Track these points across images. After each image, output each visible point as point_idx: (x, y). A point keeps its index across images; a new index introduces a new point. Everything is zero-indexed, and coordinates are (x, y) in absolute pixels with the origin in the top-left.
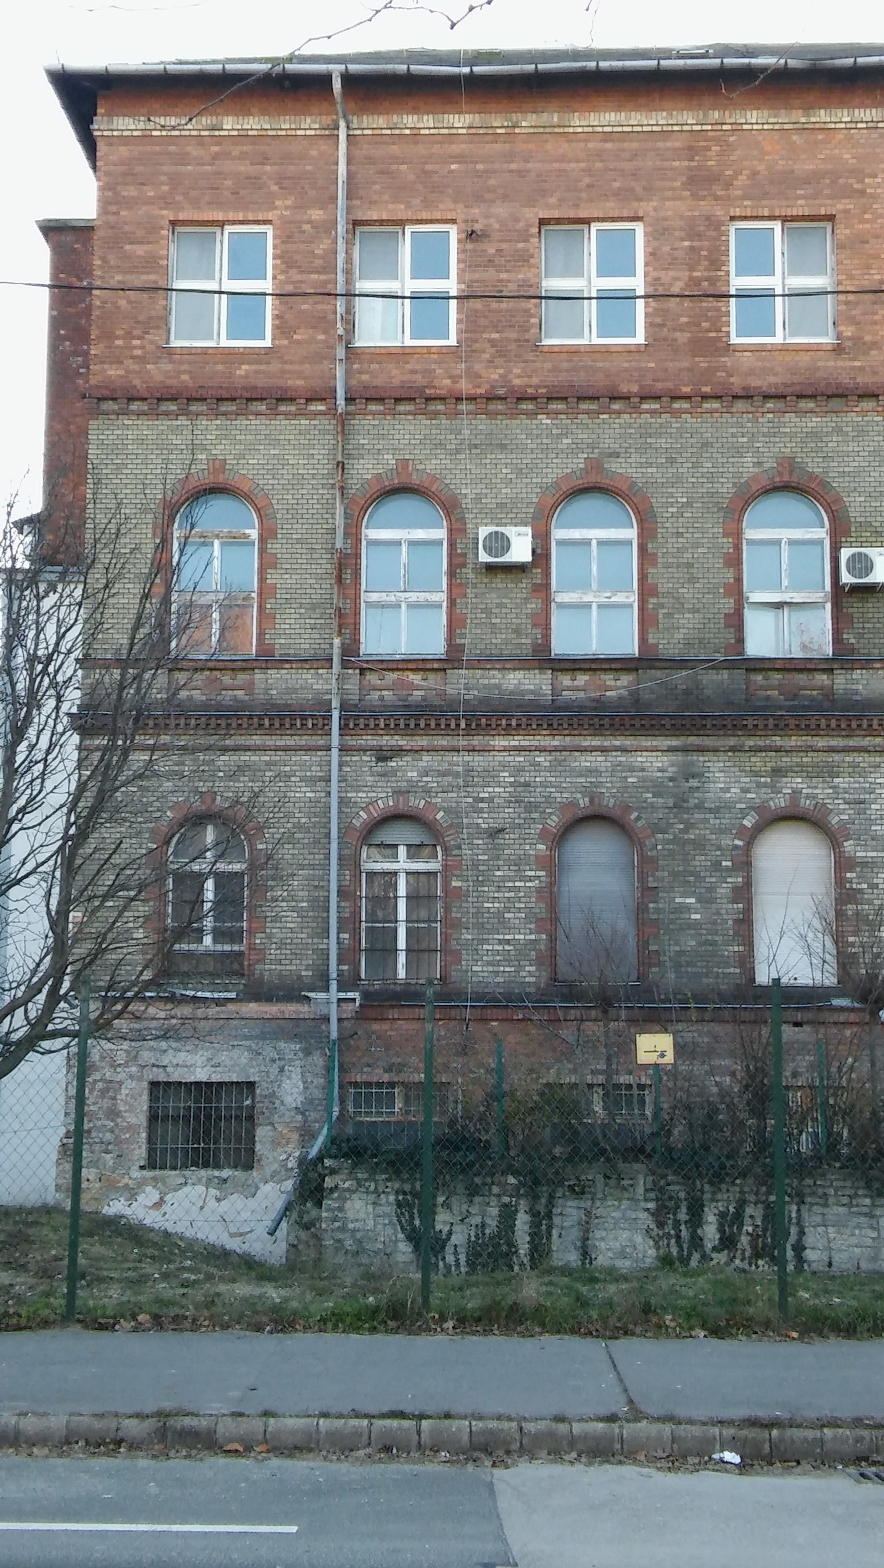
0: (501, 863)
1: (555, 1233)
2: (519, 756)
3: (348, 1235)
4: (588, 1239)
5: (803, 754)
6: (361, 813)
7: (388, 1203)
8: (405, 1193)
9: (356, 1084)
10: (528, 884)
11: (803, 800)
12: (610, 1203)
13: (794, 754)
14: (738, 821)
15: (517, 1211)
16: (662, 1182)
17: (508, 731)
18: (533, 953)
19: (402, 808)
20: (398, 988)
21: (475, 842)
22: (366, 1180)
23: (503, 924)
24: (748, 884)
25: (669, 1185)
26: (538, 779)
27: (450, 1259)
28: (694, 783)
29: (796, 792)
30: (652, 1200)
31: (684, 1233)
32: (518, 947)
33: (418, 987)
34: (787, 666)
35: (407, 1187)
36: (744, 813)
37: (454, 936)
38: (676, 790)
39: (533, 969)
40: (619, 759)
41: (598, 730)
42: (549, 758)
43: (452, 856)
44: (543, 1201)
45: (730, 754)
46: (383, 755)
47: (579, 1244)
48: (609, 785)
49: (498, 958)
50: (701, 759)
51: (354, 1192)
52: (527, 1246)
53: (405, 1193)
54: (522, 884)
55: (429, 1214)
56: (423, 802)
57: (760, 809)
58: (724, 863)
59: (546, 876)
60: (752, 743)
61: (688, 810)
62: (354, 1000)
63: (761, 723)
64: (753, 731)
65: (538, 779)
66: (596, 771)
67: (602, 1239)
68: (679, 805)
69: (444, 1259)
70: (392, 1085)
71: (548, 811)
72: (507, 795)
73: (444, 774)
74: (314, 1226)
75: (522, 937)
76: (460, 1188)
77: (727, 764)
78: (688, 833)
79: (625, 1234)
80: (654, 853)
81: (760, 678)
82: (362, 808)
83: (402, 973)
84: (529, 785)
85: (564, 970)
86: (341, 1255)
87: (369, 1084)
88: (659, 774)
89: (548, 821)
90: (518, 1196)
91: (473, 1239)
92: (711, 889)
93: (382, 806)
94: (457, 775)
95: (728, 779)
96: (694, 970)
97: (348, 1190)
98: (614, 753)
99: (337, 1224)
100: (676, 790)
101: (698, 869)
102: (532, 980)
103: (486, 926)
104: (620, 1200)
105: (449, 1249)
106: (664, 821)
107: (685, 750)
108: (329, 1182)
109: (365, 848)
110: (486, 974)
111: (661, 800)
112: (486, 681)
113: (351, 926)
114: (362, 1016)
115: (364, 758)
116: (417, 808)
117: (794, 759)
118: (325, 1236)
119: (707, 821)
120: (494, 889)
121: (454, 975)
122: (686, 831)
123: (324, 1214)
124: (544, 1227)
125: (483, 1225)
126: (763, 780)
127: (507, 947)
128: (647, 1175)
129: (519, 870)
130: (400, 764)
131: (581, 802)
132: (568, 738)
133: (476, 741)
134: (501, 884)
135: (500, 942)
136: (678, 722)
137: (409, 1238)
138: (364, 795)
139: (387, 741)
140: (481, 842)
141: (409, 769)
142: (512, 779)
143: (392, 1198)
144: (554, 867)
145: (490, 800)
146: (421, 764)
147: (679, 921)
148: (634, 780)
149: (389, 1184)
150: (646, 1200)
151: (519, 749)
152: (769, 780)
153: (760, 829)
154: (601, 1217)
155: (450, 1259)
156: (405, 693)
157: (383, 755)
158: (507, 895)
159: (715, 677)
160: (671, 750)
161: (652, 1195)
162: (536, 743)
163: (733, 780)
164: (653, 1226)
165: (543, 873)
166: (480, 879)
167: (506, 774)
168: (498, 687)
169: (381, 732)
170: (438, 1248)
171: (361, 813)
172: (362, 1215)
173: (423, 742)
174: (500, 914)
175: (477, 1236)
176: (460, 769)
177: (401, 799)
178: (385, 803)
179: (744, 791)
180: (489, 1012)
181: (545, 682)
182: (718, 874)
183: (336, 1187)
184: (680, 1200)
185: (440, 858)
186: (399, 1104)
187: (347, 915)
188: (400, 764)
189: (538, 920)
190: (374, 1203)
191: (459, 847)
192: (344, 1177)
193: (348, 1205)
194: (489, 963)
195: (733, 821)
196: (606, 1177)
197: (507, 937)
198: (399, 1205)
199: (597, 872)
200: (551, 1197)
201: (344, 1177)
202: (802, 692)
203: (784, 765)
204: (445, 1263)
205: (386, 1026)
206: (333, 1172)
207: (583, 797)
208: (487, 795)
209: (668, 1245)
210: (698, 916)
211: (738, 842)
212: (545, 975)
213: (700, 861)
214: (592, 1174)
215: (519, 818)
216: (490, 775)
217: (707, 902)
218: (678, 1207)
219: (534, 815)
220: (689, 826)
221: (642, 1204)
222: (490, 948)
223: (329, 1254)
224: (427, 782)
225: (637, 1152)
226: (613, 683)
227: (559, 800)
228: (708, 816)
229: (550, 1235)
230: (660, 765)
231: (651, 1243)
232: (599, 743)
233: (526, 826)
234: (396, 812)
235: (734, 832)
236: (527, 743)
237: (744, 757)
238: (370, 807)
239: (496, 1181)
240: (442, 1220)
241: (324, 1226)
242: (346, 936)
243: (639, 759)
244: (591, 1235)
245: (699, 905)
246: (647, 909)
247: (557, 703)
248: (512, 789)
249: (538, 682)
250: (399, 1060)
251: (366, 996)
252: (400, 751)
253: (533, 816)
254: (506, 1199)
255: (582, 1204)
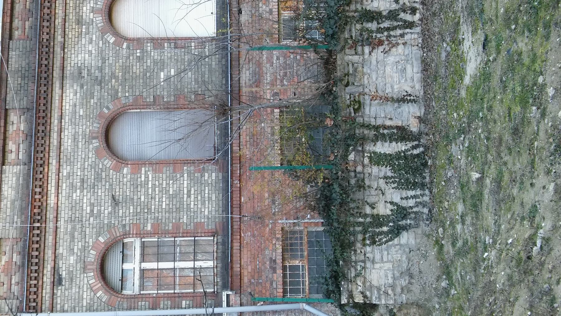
0: (135, 197)
1: (388, 123)
2: (62, 186)
3: (397, 282)
4: (392, 98)
5: (68, 5)
6: (98, 295)
7: (373, 251)
8: (364, 239)
9: (285, 292)
10: (150, 179)
11: (98, 6)
12: (366, 82)
13: (67, 11)
14: (111, 46)
15: (375, 153)
16: (350, 42)
17: (44, 193)
18: (196, 175)
19: (96, 266)
20: (219, 265)
21: (120, 215)
22: (356, 270)
23: (177, 195)
24: (153, 40)
25: (351, 37)
26: (79, 174)
27: (411, 203)
28: (85, 73)
29: (93, 10)
30: (363, 50)
31: (386, 24)
32: (192, 184)
33: (219, 251)
34: (9, 14)
35: (360, 237)
36: (106, 42)
37: (185, 227)
38: (89, 84)
39: (206, 175)
40: (67, 121)
41: (47, 134)
42: (65, 167)
43: (130, 231)
44: (366, 132)
45: (66, 50)
46: (57, 281)
47: (396, 105)
48: (84, 127)
49: (199, 198)
50: (69, 69)
51: (365, 278)
52: (399, 143)
53: (364, 239)
54: (150, 183)
55: (378, 220)
56: (92, 252)
57: (103, 33)
58: (138, 55)
59: (145, 167)
60: (59, 37)
61: (103, 77)
62: (228, 296)
63: (46, 30)
64: (52, 37)
65: (79, 174)
66: (74, 135)
67: (392, 87)
68: (100, 82)
69: (411, 208)
70: (284, 268)
71: (101, 167)
72: (89, 194)
73: (73, 237)
74: (392, 309)
75: (185, 182)
76: (359, 195)
77: (73, 52)
78: (118, 76)
79: (388, 69)
80: (131, 98)
81: (16, 33)
82: (95, 294)
83: (210, 264)
84: (83, 179)
85: (209, 153)
86: (413, 288)
87: (284, 283)
88: (78, 95)
89: (108, 166)
90: (363, 151)
91: (396, 185)
92: (155, 62)
93: (94, 281)
94: (74, 228)
95: (83, 51)
96: (207, 73)
97: (364, 283)
98: (63, 124)
99: (390, 292)
100: (89, 84)
101: (142, 70)
102: (214, 174)
103: (178, 206)
104: (364, 74)
105: (404, 203)
106: (110, 92)
107: (63, 78)
108: (359, 299)
109: (124, 292)
110: (210, 206)
111: (96, 94)
112: (8, 210)
113: (177, 299)
114: (239, 290)
115: (59, 294)
116: (95, 255)
117: (71, 11)
118: (399, 301)
119: (110, 65)
120: (153, 202)
121: (212, 227)
122: (116, 78)
123: (383, 302)
124: (386, 132)
125: (385, 178)
126: (84, 30)
127: (192, 192)
128: (345, 53)
129: (141, 185)
130: (64, 269)
131: (95, 145)
132: (51, 154)
133: (51, 215)
134: (150, 197)
135: (189, 196)
136: (43, 81)
137: (398, 234)
138: (85, 293)
139: (47, 279)
140: (121, 211)
141: (68, 262)
142: (78, 191)
143: (368, 249)
144: (139, 163)
145: (92, 205)
146: (65, 254)
147: (176, 83)
148: (81, 110)
149: (359, 251)
150: (363, 54)
151: (58, 186)
152: (84, 27)
153: (116, 33)
154: (376, 88)
155: (411, 203)
156: (14, 265)
157: (57, 281)
158: (157, 193)
159: (14, 60)
160: (62, 88)
161: (359, 49)
162: (54, 175)
163: (83, 49)
164: (381, 48)
165: (143, 169)
166: (146, 211)
167: (74, 195)
168: (13, 202)
169: (40, 283)
170: (405, 212)
171: (98, 295)
172: (382, 273)
173: (49, 254)
174: (171, 198)
175: (394, 182)
176: (69, 227)
177: (89, 267)
178: (92, 278)
179: (91, 41)
180: (234, 203)
181: (11, 170)
182: (145, 58)
183: (362, 293)
184: (363, 28)
185: (133, 240)
186: (297, 263)
187: (169, 303)
188: (64, 269)
189: (174, 171)
190: (373, 264)
191: (124, 226)
192: (354, 287)
193: (375, 283)
194: (203, 203)
195: (111, 49)
196: (347, 85)
197: (185, 192)
198: (373, 243)
199: (142, 135)
200: (363, 126)
201: (354, 287)
202: (27, 7)
203: (74, 18)
204: (415, 207)
205: (245, 273)
206: (351, 296)
207: (92, 143)
208: (88, 208)
209: (395, 37)
210: (172, 71)
211: (125, 44)
212: (210, 166)
213: (137, 69)
214: (345, 95)
215: (105, 185)
216: (74, 206)
217: (163, 65)
218: (367, 29)
219: (104, 176)
220: (113, 76)
221: (366, 56)
222: (192, 203)
223: (413, 298)
224: (78, 249)
225: (329, 63)
226: (15, 126)
227: (93, 160)
228: (107, 64)
229: (390, 127)
230: (72, 95)
231: (394, 49)
232: (55, 134)
233: (111, 181)
234: (99, 270)
235: (118, 48)
236: (54, 181)
237: (69, 42)
238: (94, 289)
239: (352, 169)
240: (384, 210)
241: (392, 302)
242: (184, 302)
243: (67, 108)
244: (390, 95)
245: (166, 70)
246: (168, 102)
247: (27, 162)
248: (85, 191)
249: (11, 175)
250: (268, 263)
251: (225, 287)
252: (55, 269)
253: (104, 176)
254: (366, 161)
255: (368, 102)
